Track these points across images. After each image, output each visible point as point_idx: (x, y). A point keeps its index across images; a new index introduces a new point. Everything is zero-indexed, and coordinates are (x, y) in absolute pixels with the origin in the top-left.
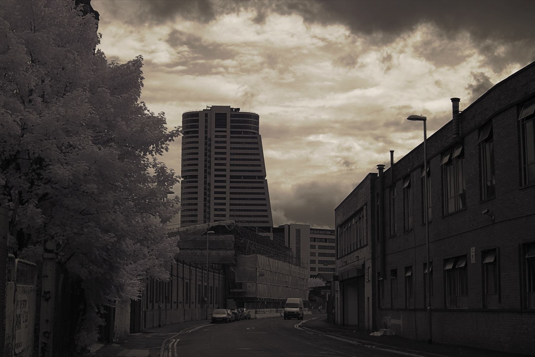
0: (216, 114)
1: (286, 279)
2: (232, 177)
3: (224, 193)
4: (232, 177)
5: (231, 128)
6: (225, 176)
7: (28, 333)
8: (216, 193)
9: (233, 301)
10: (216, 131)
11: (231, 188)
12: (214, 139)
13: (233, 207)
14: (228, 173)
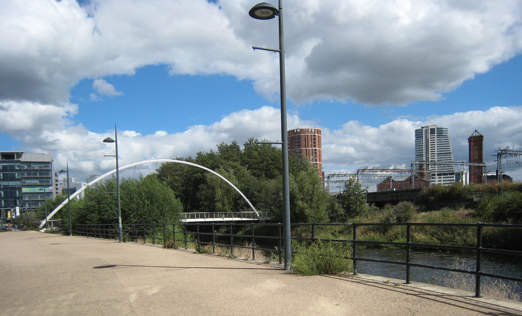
0: (430, 129)
1: (412, 187)
2: (438, 154)
3: (435, 145)
4: (438, 154)
5: (437, 134)
6: (435, 154)
7: (184, 257)
8: (431, 152)
9: (473, 297)
10: (431, 136)
11: (437, 149)
12: (430, 139)
13: (438, 157)
14: (436, 153)
